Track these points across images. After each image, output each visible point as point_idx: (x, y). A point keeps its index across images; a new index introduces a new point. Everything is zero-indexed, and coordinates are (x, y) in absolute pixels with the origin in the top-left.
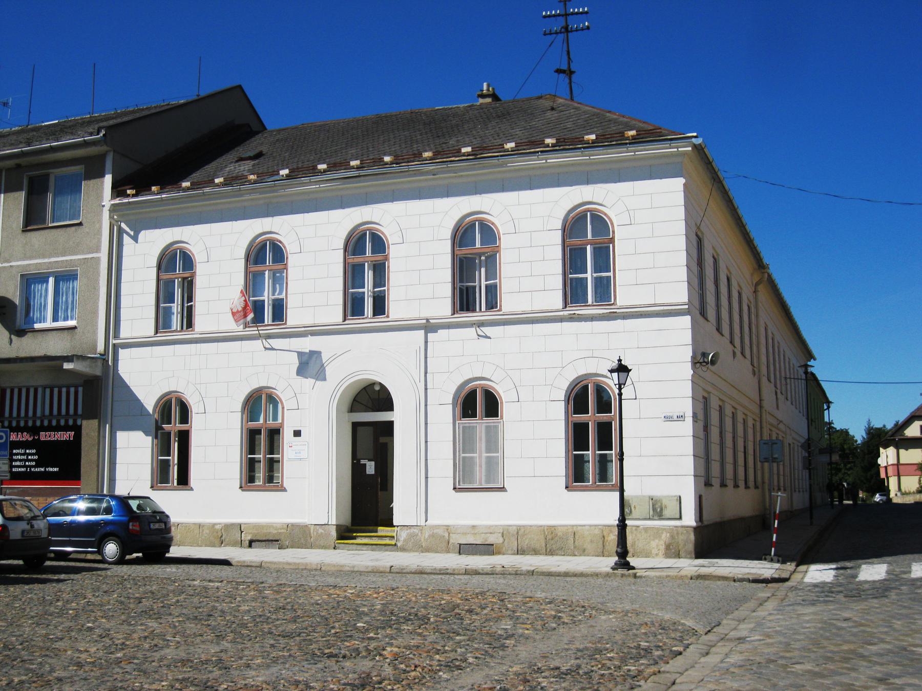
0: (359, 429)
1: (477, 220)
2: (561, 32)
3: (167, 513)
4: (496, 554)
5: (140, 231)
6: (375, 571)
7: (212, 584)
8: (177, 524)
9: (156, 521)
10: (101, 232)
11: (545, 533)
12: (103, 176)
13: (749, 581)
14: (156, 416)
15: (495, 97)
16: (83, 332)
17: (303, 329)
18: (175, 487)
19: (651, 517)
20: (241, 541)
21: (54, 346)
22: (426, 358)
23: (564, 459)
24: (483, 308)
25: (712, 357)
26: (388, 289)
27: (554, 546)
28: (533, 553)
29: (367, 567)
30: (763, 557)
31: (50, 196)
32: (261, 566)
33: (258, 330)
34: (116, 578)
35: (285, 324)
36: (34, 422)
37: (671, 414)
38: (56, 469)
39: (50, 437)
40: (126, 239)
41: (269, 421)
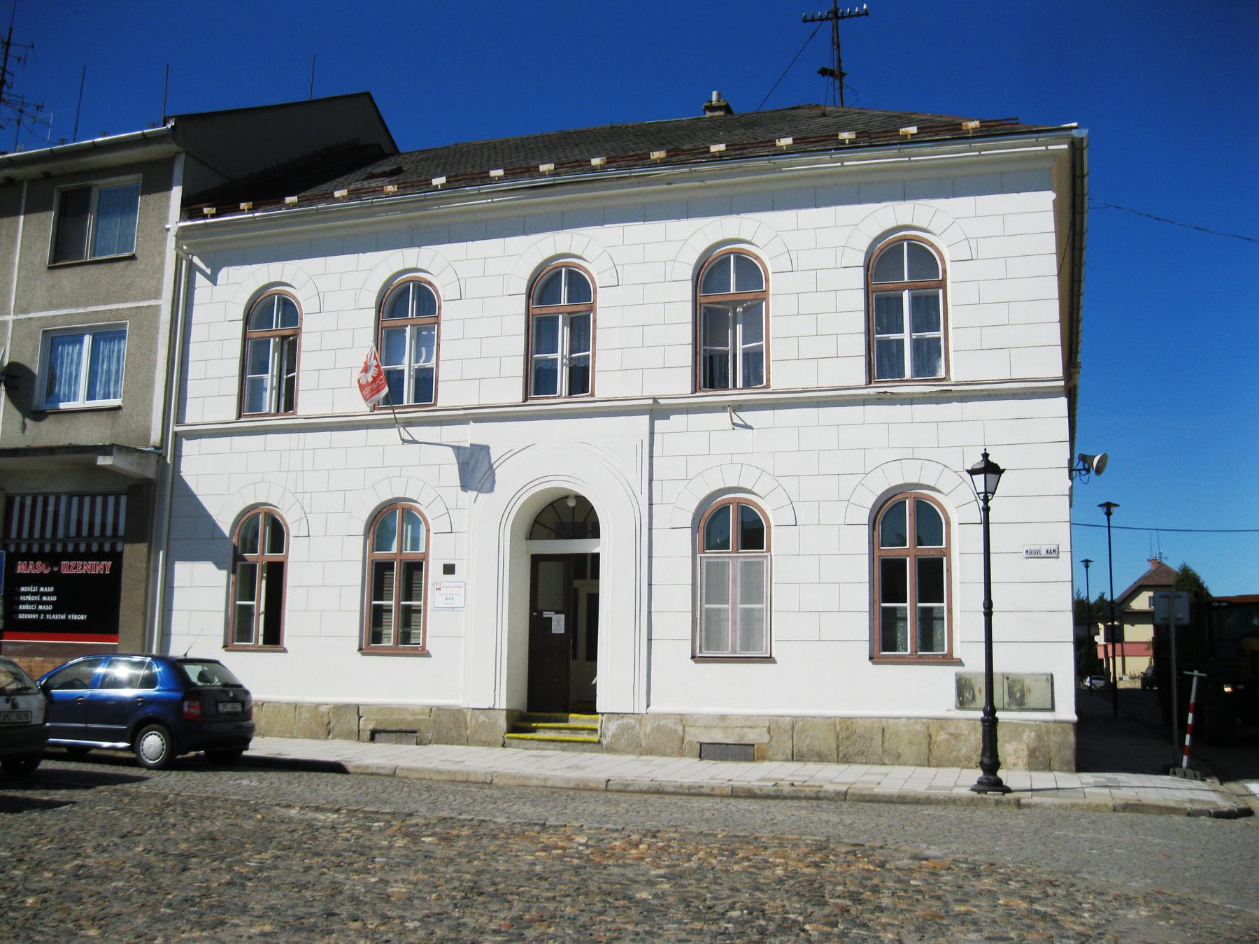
0: (543, 565)
1: (732, 253)
2: (827, 19)
3: (247, 686)
4: (758, 759)
5: (220, 269)
6: (581, 786)
7: (321, 816)
8: (261, 703)
9: (226, 699)
10: (163, 269)
11: (836, 728)
12: (169, 188)
13: (1209, 814)
14: (234, 540)
15: (727, 109)
16: (131, 416)
17: (462, 412)
18: (260, 647)
19: (1006, 706)
20: (359, 731)
21: (87, 434)
22: (651, 457)
23: (868, 614)
24: (740, 383)
25: (1098, 462)
26: (594, 354)
27: (850, 750)
28: (818, 759)
29: (569, 780)
30: (1171, 771)
31: (91, 219)
32: (393, 775)
33: (394, 413)
34: (152, 801)
35: (435, 404)
36: (53, 546)
37: (1037, 548)
38: (82, 617)
39: (75, 568)
40: (200, 280)
41: (406, 550)
